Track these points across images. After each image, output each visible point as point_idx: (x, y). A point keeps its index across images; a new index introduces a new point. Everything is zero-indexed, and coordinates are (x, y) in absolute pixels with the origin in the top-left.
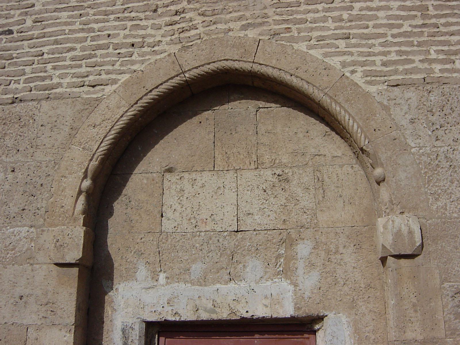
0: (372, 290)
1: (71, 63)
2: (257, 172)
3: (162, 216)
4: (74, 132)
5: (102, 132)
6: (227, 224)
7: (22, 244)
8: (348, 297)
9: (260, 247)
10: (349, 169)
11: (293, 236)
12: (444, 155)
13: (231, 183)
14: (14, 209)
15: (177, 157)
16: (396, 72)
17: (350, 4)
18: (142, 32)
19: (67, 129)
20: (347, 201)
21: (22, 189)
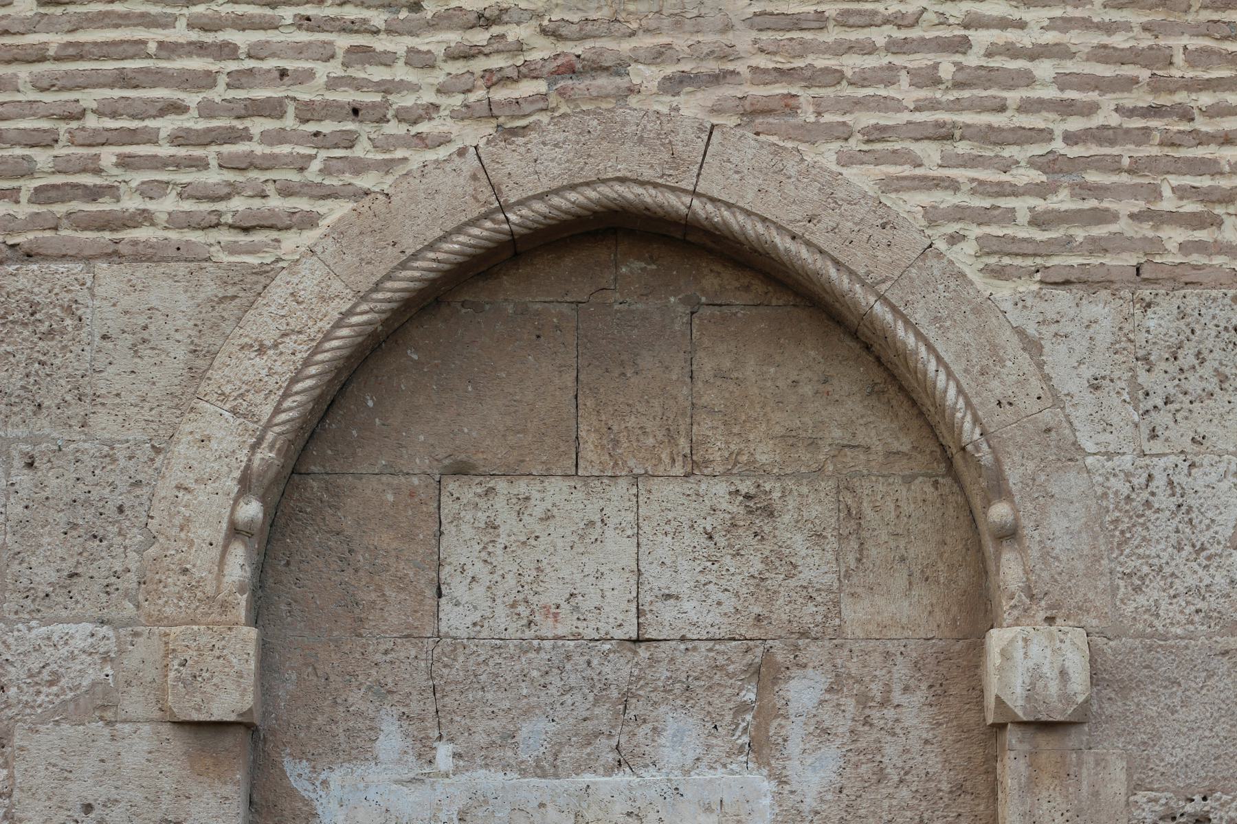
0: (968, 797)
1: (173, 151)
2: (690, 486)
3: (440, 595)
4: (201, 363)
5: (285, 369)
6: (611, 620)
7: (79, 667)
8: (909, 814)
9: (697, 683)
10: (929, 489)
11: (779, 658)
12: (1165, 478)
13: (623, 512)
14: (45, 575)
15: (474, 434)
16: (1067, 244)
17: (963, 32)
18: (377, 74)
19: (181, 352)
20: (917, 574)
21: (62, 518)
